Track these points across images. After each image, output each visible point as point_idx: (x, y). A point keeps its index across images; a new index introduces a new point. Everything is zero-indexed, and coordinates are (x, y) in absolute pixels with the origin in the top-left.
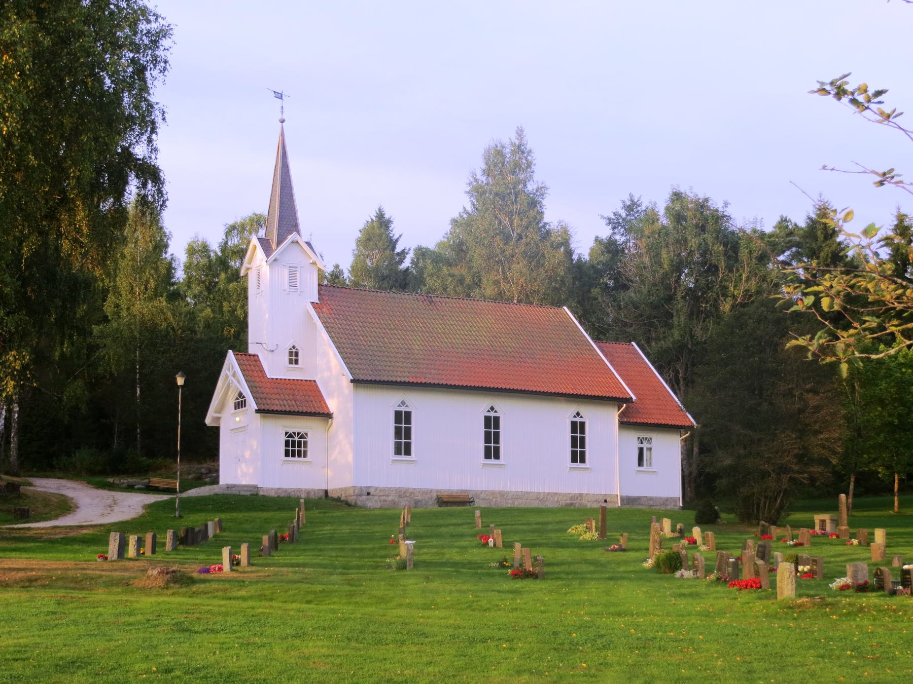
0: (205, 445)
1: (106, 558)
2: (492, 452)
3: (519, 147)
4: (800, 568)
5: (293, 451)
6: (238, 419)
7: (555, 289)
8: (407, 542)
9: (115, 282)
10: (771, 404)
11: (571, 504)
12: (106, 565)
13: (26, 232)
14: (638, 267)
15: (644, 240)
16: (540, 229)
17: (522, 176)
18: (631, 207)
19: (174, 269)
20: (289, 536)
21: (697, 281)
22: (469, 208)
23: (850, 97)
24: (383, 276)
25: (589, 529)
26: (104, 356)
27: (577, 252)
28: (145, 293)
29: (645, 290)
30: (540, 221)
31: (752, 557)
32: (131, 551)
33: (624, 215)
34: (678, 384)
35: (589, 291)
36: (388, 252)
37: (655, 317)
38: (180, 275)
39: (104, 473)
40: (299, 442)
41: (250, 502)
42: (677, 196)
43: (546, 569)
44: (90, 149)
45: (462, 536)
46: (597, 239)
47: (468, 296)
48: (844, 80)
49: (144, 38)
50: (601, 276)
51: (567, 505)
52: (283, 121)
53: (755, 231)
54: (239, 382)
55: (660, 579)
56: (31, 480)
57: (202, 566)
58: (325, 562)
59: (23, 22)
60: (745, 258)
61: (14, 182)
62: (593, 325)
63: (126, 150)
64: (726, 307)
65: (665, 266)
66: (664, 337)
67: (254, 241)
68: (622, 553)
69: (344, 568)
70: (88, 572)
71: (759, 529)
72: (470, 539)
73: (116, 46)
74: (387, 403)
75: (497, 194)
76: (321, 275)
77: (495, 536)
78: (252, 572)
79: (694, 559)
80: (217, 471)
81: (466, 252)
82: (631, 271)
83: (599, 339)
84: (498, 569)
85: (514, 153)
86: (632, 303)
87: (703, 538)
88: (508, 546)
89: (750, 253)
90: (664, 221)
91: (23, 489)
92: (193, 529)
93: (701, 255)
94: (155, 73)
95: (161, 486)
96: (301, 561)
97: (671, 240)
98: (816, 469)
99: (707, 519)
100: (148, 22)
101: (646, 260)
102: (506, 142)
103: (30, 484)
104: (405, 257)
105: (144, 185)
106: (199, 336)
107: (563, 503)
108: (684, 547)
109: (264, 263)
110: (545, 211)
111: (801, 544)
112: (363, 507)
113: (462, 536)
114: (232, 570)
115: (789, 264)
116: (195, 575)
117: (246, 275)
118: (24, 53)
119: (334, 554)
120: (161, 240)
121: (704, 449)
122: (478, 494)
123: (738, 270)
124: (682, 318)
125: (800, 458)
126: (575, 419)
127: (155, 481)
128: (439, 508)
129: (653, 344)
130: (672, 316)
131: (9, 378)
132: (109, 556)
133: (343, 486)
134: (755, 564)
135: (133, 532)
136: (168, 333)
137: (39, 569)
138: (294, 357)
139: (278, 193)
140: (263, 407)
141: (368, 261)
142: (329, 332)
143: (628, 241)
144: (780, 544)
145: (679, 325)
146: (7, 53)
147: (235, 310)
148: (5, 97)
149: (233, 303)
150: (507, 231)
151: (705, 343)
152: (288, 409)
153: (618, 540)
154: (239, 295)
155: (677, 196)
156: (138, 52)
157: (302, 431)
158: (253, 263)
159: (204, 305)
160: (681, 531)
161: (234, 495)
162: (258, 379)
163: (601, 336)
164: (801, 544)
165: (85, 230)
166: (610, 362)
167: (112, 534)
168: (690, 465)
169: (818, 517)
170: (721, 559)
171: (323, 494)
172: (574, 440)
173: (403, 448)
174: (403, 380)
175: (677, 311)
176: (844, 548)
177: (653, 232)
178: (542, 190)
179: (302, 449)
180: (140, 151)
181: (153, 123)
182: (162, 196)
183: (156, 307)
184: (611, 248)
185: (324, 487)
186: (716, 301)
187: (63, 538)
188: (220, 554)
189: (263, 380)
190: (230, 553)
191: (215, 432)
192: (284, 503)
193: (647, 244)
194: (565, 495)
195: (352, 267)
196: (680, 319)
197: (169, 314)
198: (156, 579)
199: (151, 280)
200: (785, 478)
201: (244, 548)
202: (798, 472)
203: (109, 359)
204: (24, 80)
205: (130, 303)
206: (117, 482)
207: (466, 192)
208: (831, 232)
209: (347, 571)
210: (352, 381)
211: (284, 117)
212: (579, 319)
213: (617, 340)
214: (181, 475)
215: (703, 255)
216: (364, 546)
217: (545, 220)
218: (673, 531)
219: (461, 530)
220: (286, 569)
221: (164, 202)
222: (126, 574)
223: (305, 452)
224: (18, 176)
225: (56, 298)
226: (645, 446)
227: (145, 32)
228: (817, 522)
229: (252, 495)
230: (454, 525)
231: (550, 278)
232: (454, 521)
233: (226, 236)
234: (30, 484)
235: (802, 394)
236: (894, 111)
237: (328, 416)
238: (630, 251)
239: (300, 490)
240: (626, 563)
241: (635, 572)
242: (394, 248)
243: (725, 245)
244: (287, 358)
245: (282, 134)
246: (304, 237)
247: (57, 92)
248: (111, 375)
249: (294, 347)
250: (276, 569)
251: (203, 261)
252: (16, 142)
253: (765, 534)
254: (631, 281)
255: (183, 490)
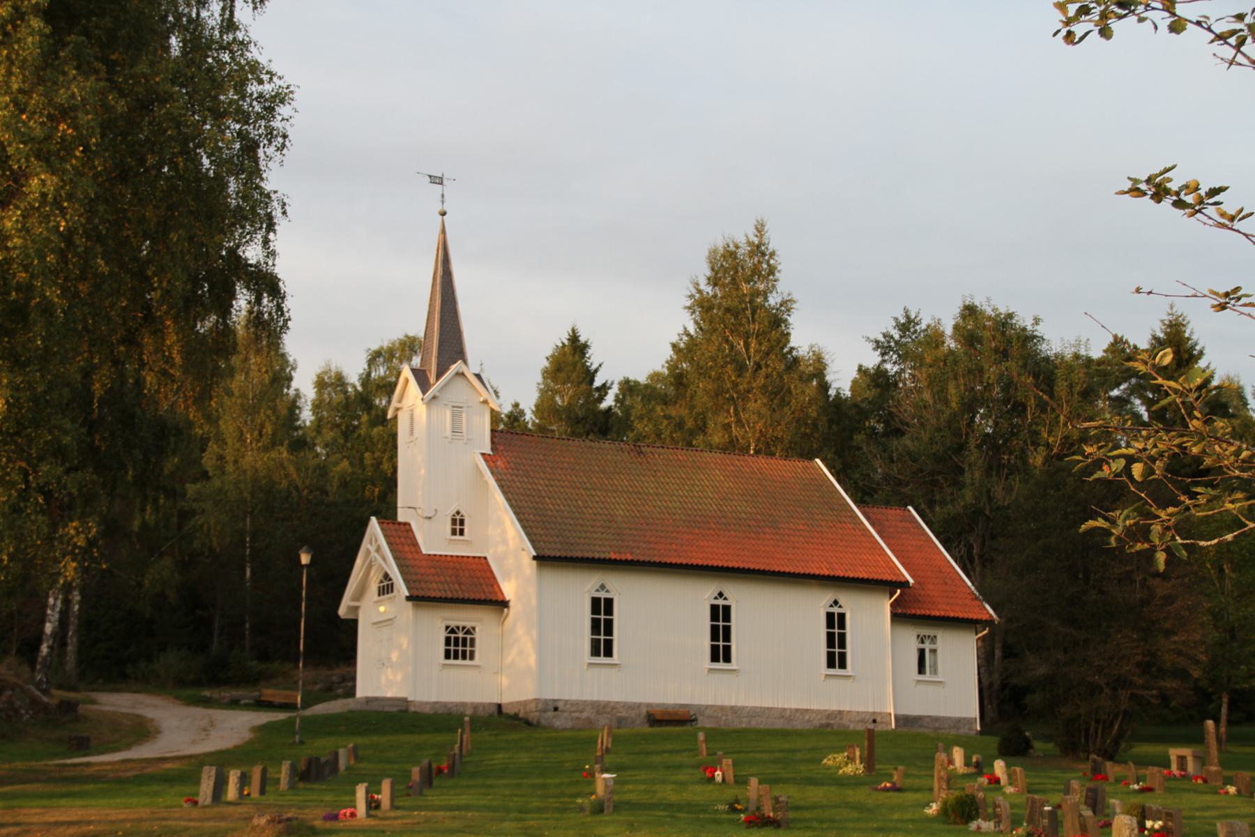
0: (338, 644)
1: (196, 803)
2: (721, 653)
3: (758, 247)
4: (1149, 824)
5: (456, 652)
6: (382, 609)
7: (805, 435)
8: (606, 776)
9: (218, 426)
10: (1101, 592)
11: (828, 725)
12: (195, 813)
13: (96, 361)
14: (916, 406)
15: (924, 369)
16: (784, 356)
17: (762, 287)
18: (906, 326)
19: (299, 408)
20: (448, 767)
21: (996, 424)
22: (692, 329)
23: (1175, 198)
24: (577, 418)
25: (851, 759)
26: (202, 526)
27: (834, 385)
28: (258, 441)
29: (925, 436)
30: (785, 345)
31: (1076, 805)
32: (232, 792)
33: (897, 337)
34: (972, 562)
35: (851, 438)
36: (584, 387)
37: (939, 473)
38: (307, 416)
39: (197, 683)
40: (464, 640)
41: (398, 719)
42: (970, 311)
43: (791, 815)
44: (182, 252)
45: (680, 767)
46: (861, 369)
47: (690, 444)
48: (1166, 175)
49: (255, 103)
50: (867, 418)
51: (822, 726)
52: (443, 214)
53: (1077, 356)
54: (384, 559)
55: (949, 831)
56: (95, 695)
57: (328, 810)
58: (495, 803)
59: (87, 79)
60: (1063, 394)
61: (76, 294)
62: (856, 483)
63: (233, 252)
64: (1037, 459)
65: (954, 405)
66: (953, 500)
67: (406, 372)
68: (896, 794)
69: (521, 812)
70: (170, 823)
71: (1087, 767)
72: (690, 771)
73: (219, 115)
74: (580, 589)
75: (728, 310)
76: (495, 417)
77: (725, 768)
78: (396, 818)
79: (995, 806)
80: (354, 679)
81: (686, 387)
82: (907, 410)
83: (864, 502)
84: (727, 813)
85: (752, 254)
86: (909, 453)
87: (1010, 776)
88: (741, 781)
89: (1071, 386)
90: (951, 344)
91: (82, 709)
92: (318, 759)
93: (1003, 390)
94: (271, 150)
95: (277, 700)
96: (463, 802)
97: (961, 369)
98: (1170, 684)
99: (1015, 749)
100: (261, 82)
101: (927, 395)
102: (742, 240)
103: (93, 702)
104: (606, 394)
105: (259, 300)
106: (331, 498)
107: (817, 723)
108: (981, 788)
109: (419, 402)
110: (792, 331)
111: (1150, 790)
112: (550, 728)
113: (680, 767)
114: (369, 815)
115: (1127, 401)
116: (318, 823)
117: (395, 417)
118: (88, 122)
119: (507, 792)
120: (283, 369)
121: (1010, 653)
122: (702, 709)
123: (1053, 410)
124: (977, 475)
125: (1145, 668)
126: (831, 610)
127: (269, 693)
128: (651, 729)
129: (938, 509)
130: (962, 471)
131: (68, 558)
132: (201, 799)
133: (523, 698)
134: (1080, 815)
135: (234, 765)
136: (291, 493)
137: (99, 822)
138: (458, 526)
139: (438, 308)
140: (416, 593)
141: (558, 399)
142: (505, 493)
143: (903, 371)
144: (1120, 787)
145: (973, 484)
146: (65, 121)
147: (381, 463)
148: (62, 180)
149: (377, 454)
150: (740, 359)
151: (1008, 508)
152: (449, 595)
153: (891, 776)
154: (386, 443)
155: (970, 311)
156: (247, 123)
157: (468, 625)
158: (404, 402)
159: (339, 456)
160: (978, 765)
161: (376, 712)
162: (409, 556)
163: (867, 498)
164: (1150, 790)
165: (178, 360)
166: (879, 532)
167: (206, 768)
168: (990, 673)
169: (1174, 753)
170: (1032, 807)
171: (495, 709)
172: (830, 637)
173: (602, 647)
174: (602, 556)
175: (970, 465)
176: (1216, 797)
177: (936, 360)
178: (787, 304)
179: (468, 649)
180: (252, 253)
181: (270, 217)
182: (282, 314)
183: (274, 460)
184: (876, 380)
185: (496, 700)
186: (1023, 451)
187: (136, 777)
188: (354, 793)
189: (417, 556)
190: (367, 792)
191: (351, 626)
192: (442, 721)
193: (929, 376)
194: (819, 712)
195: (537, 406)
196: (973, 476)
197: (292, 469)
198: (263, 830)
199: (267, 424)
200: (1124, 695)
201: (386, 785)
202: (1143, 687)
203: (209, 529)
204: (89, 159)
205: (238, 453)
206: (216, 696)
207: (686, 308)
208: (1186, 356)
209: (523, 816)
210: (535, 558)
211: (446, 208)
212: (837, 475)
213: (887, 503)
214: (304, 685)
215: (1005, 389)
216: (549, 781)
217: (792, 344)
218: (967, 763)
219: (678, 759)
220: (441, 813)
221: (286, 321)
222: (223, 824)
223: (472, 653)
224: (83, 288)
225: (128, 448)
226: (927, 646)
227: (255, 95)
228: (1173, 758)
229: (401, 711)
230: (671, 752)
231: (797, 421)
232: (670, 746)
233: (369, 366)
234: (93, 702)
235: (1145, 580)
236: (1241, 210)
237: (504, 604)
238: (905, 384)
239: (464, 704)
240: (902, 807)
241: (913, 821)
242: (592, 381)
243: (1036, 376)
244: (449, 527)
245: (443, 231)
246: (473, 367)
247: (137, 174)
248: (211, 550)
249: (458, 513)
250: (429, 814)
251: (337, 398)
252: (80, 241)
253: (1097, 773)
254: (907, 425)
255: (307, 704)
